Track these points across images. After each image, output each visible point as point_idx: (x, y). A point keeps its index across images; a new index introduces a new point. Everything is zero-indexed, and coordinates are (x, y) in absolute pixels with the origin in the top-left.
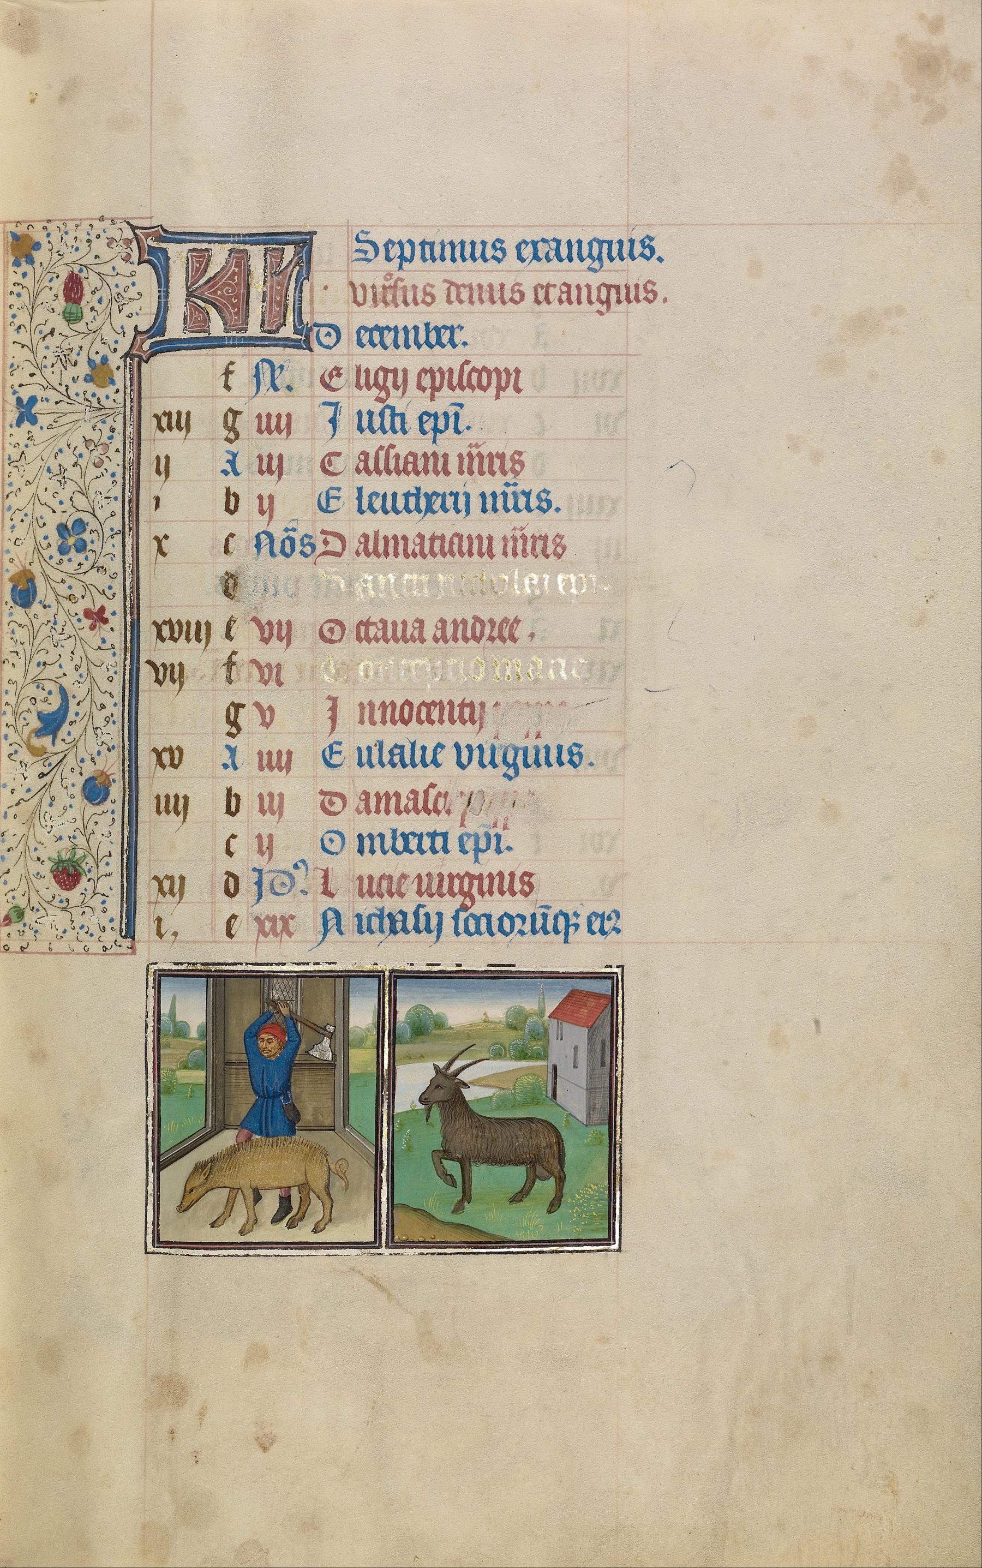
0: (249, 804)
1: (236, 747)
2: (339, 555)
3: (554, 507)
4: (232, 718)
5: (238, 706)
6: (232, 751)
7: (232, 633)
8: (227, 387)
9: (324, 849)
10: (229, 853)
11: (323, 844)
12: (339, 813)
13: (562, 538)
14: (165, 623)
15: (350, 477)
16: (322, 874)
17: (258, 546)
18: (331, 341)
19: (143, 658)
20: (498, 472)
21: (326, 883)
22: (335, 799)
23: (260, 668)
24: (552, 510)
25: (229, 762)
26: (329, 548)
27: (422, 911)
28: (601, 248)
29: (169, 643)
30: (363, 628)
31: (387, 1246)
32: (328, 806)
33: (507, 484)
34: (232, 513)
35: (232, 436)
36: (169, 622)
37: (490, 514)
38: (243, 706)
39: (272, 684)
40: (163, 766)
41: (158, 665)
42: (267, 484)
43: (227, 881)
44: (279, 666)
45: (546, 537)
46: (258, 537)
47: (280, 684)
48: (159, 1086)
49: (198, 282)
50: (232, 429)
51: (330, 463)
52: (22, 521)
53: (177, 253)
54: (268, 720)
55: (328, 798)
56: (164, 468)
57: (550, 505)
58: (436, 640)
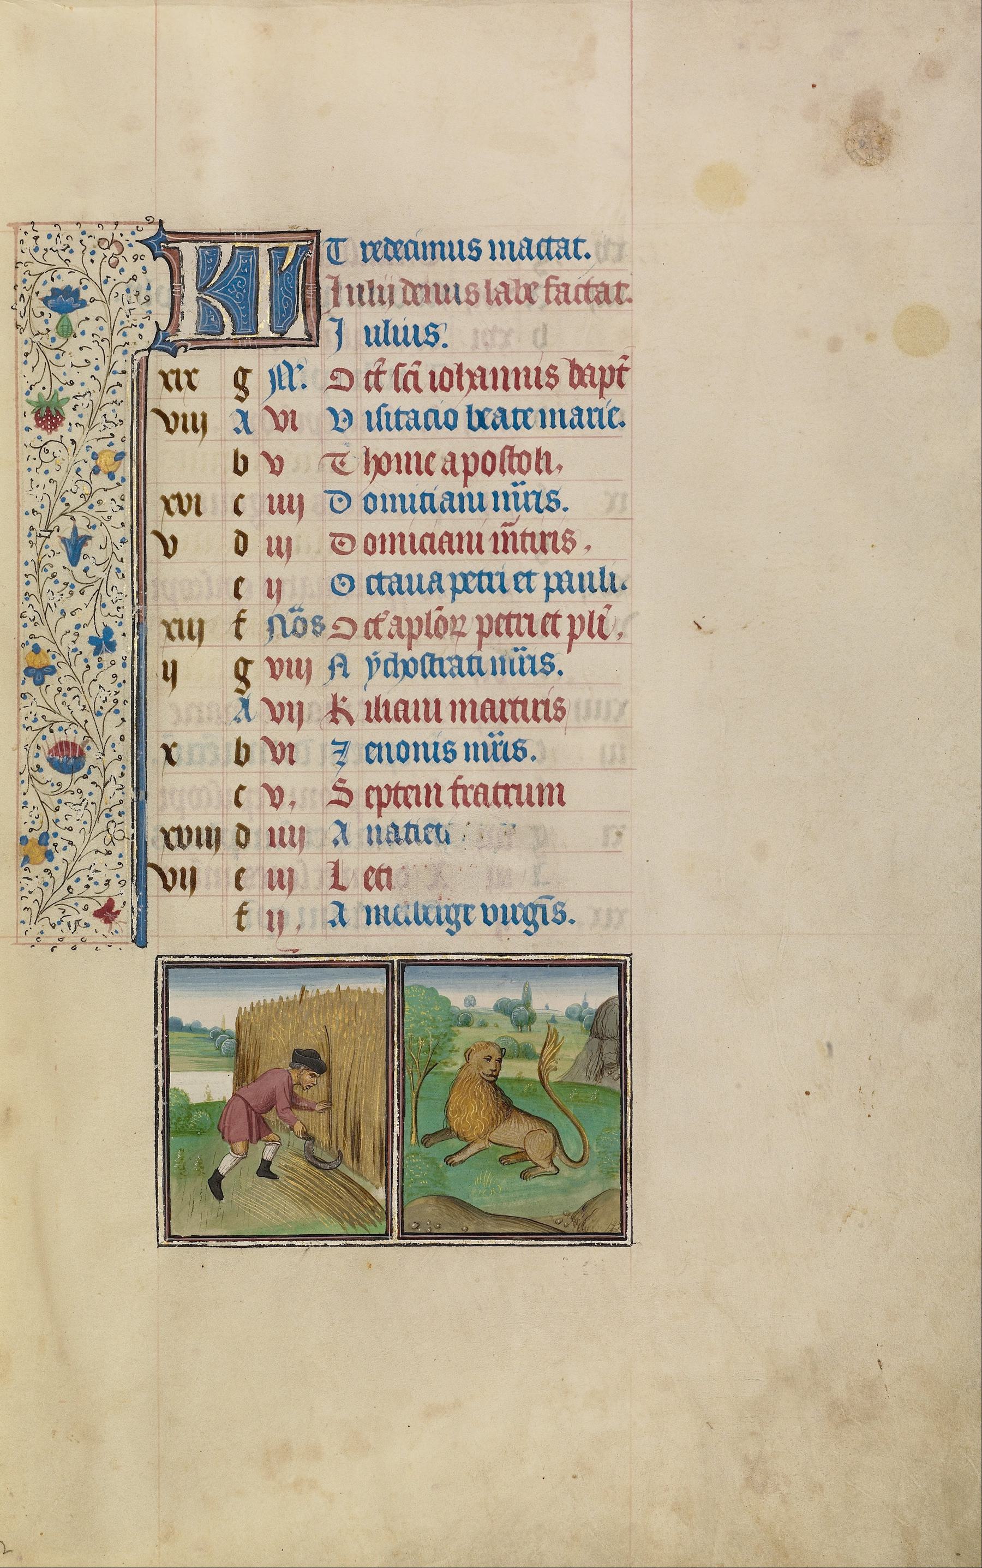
0: (256, 545)
1: (247, 412)
2: (347, 389)
3: (568, 919)
4: (241, 673)
5: (245, 372)
6: (244, 415)
7: (241, 883)
8: (238, 636)
9: (334, 590)
10: (238, 512)
11: (333, 585)
12: (346, 594)
13: (572, 533)
14: (173, 829)
15: (361, 532)
16: (333, 866)
17: (271, 630)
18: (345, 590)
19: (149, 530)
20: (510, 720)
21: (336, 875)
22: (345, 540)
23: (271, 791)
24: (566, 922)
25: (241, 427)
26: (340, 631)
27: (383, 410)
28: (535, 913)
29: (178, 850)
30: (371, 626)
31: (392, 962)
32: (339, 547)
33: (515, 484)
34: (241, 553)
35: (242, 394)
36: (178, 497)
37: (501, 555)
38: (251, 662)
39: (285, 762)
40: (172, 638)
41: (169, 414)
42: (276, 568)
43: (238, 835)
44: (291, 746)
45: (555, 534)
46: (271, 621)
47: (292, 762)
48: (167, 1108)
49: (211, 281)
50: (242, 387)
51: (342, 464)
52: (29, 470)
53: (189, 251)
54: (277, 801)
55: (338, 539)
56: (171, 674)
57: (564, 917)
58: (445, 471)
